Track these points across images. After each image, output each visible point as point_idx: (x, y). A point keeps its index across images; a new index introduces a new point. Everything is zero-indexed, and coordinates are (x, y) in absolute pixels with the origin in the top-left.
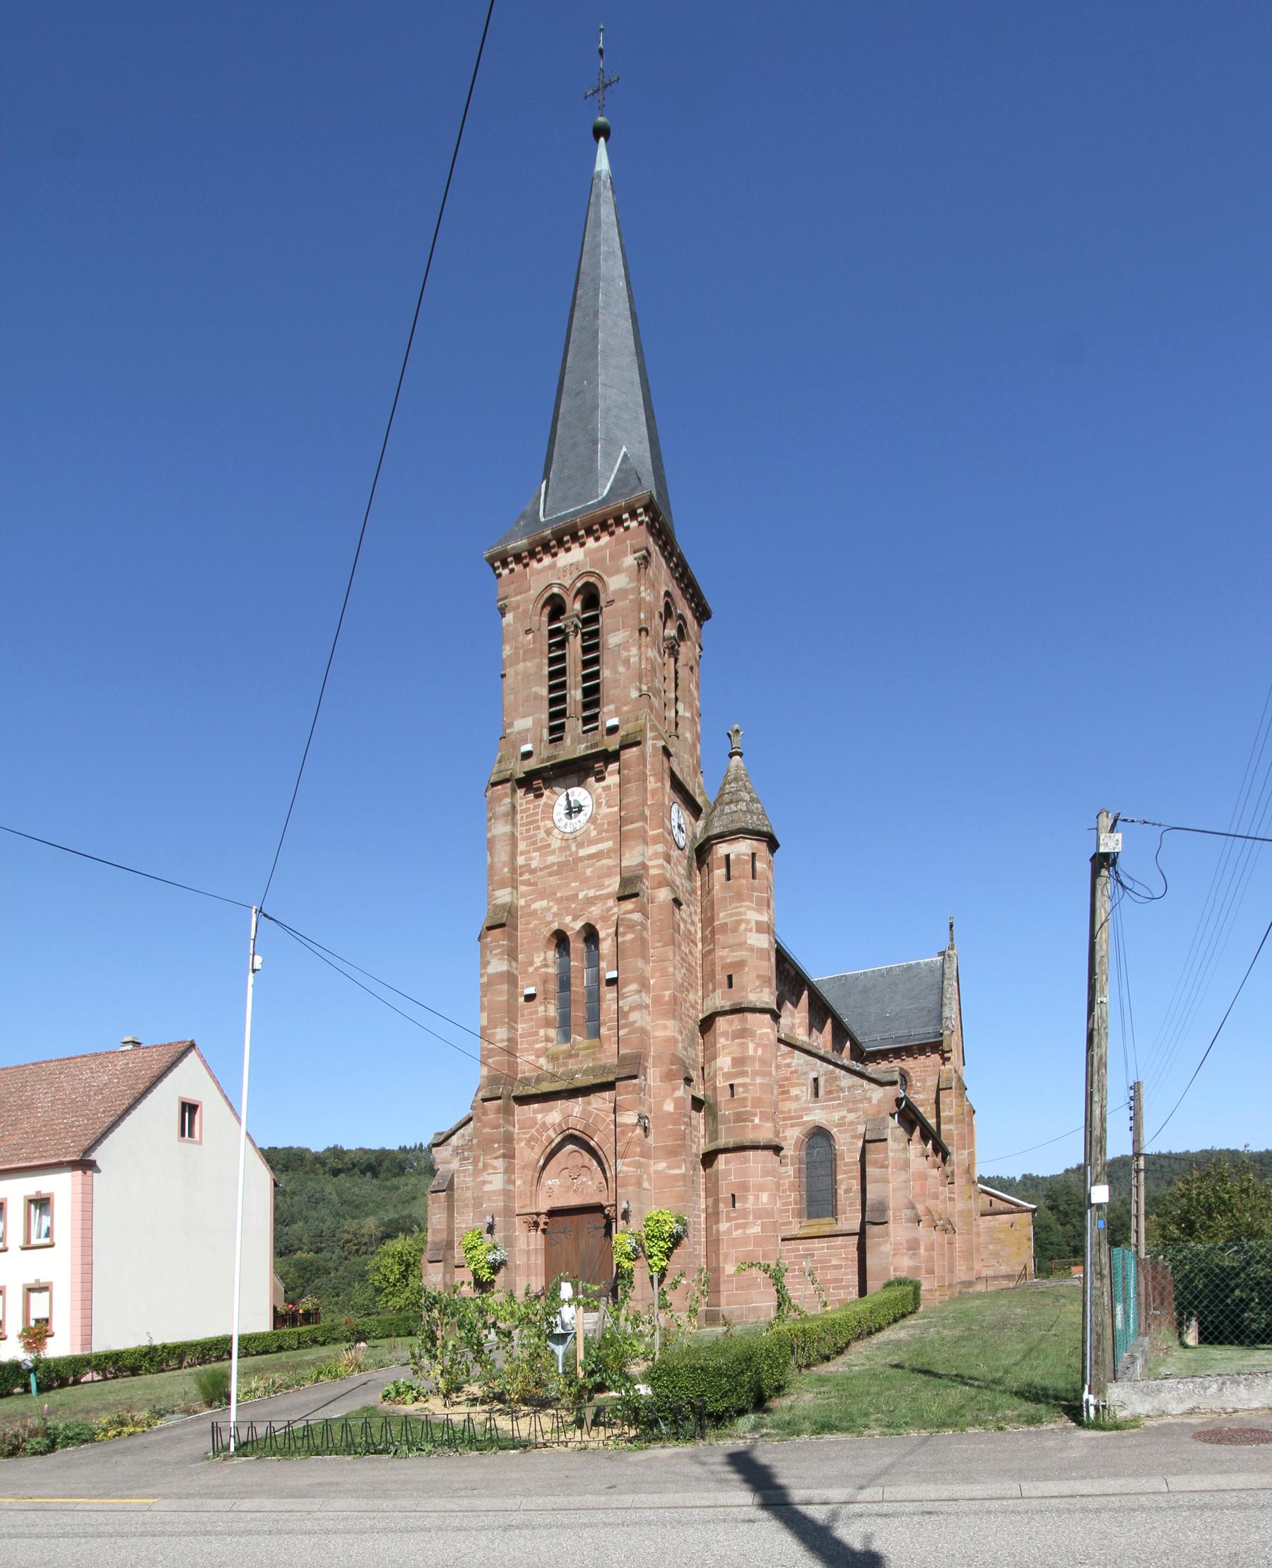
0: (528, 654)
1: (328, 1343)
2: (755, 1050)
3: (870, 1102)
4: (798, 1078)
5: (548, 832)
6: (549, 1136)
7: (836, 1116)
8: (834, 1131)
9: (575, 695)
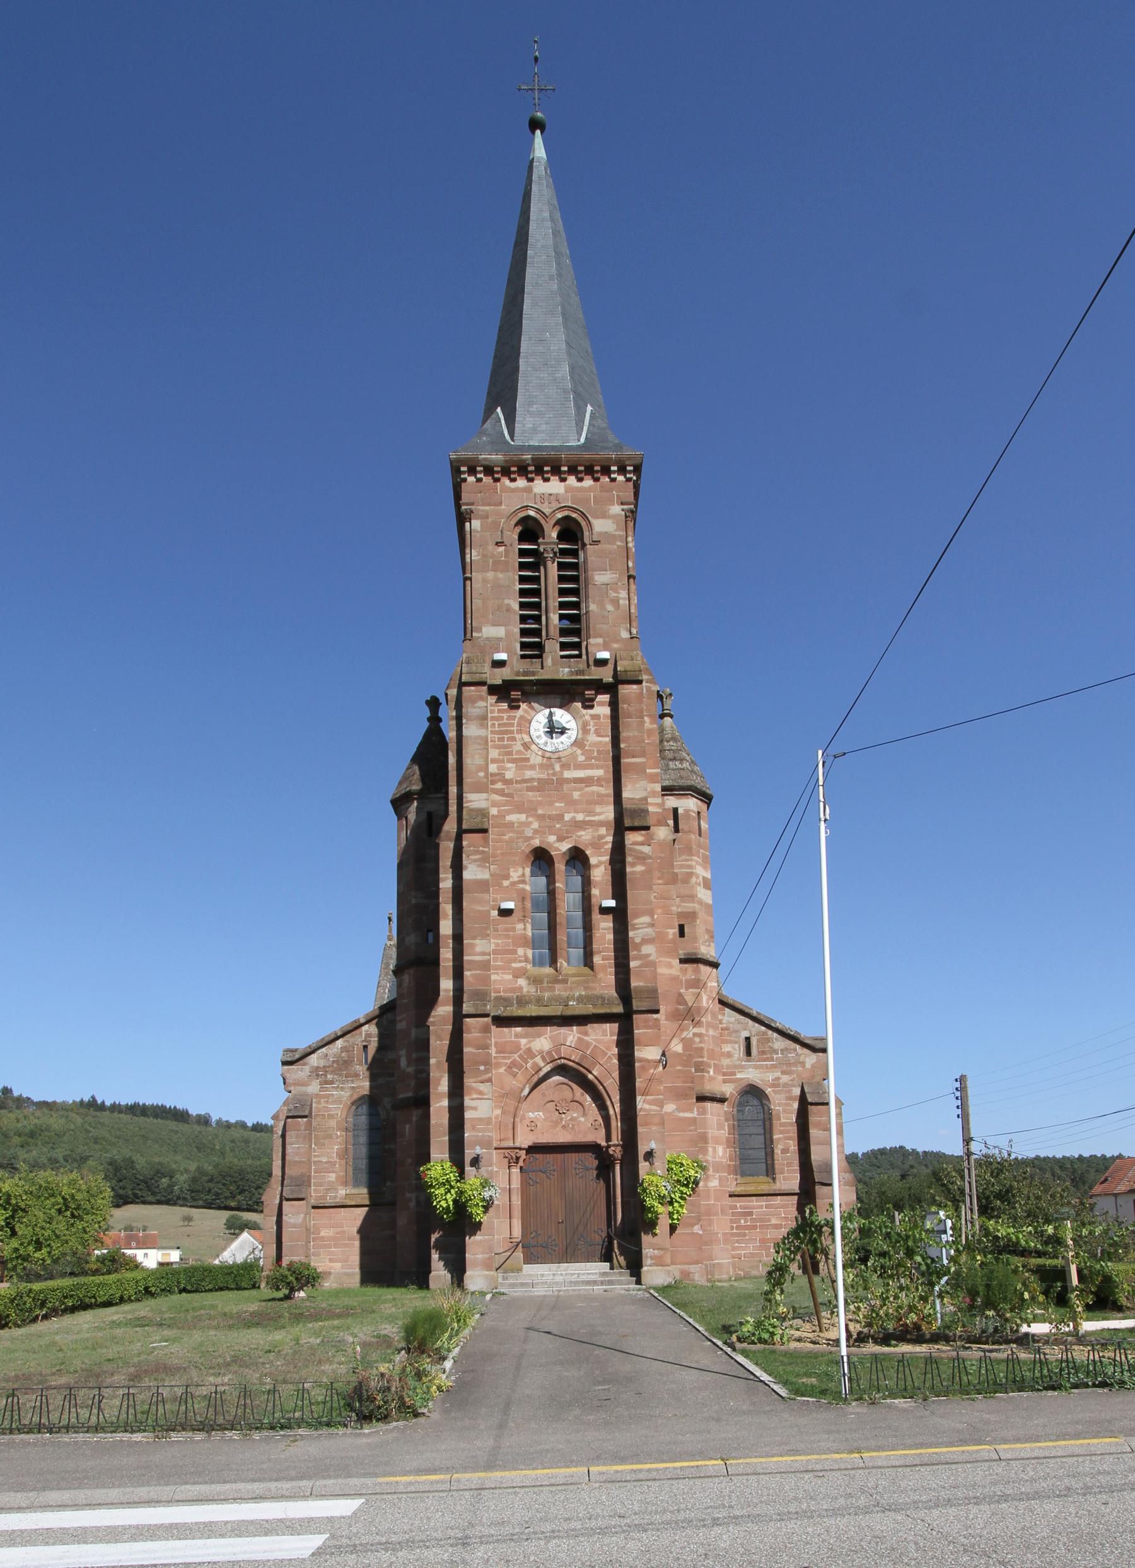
0: (497, 566)
1: (777, 1274)
3: (804, 1066)
4: (730, 1035)
5: (526, 746)
6: (535, 1064)
7: (770, 1076)
8: (768, 1091)
9: (554, 619)
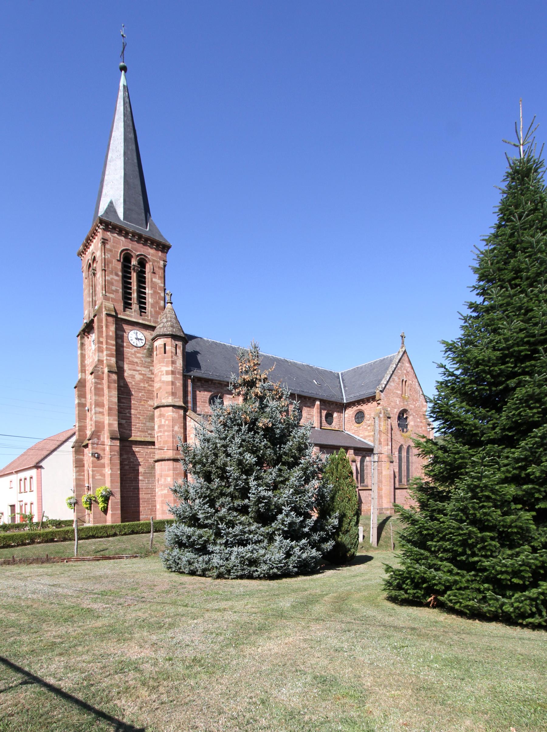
2: (165, 422)
